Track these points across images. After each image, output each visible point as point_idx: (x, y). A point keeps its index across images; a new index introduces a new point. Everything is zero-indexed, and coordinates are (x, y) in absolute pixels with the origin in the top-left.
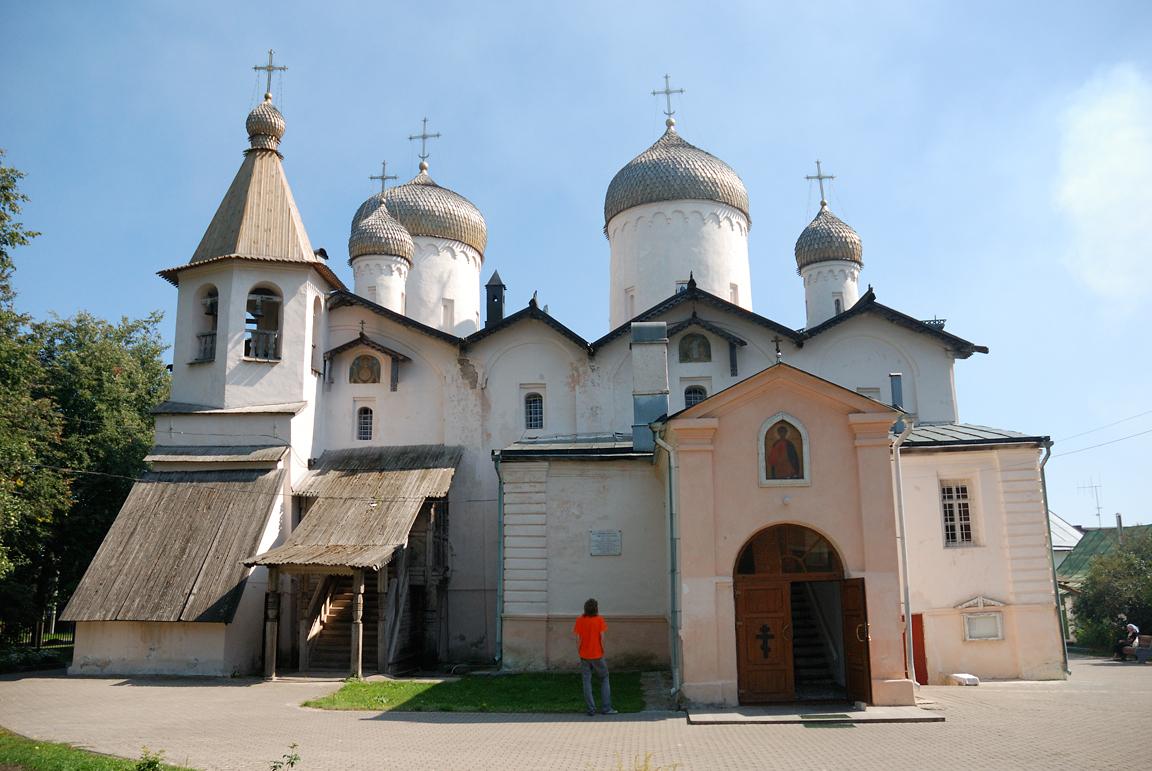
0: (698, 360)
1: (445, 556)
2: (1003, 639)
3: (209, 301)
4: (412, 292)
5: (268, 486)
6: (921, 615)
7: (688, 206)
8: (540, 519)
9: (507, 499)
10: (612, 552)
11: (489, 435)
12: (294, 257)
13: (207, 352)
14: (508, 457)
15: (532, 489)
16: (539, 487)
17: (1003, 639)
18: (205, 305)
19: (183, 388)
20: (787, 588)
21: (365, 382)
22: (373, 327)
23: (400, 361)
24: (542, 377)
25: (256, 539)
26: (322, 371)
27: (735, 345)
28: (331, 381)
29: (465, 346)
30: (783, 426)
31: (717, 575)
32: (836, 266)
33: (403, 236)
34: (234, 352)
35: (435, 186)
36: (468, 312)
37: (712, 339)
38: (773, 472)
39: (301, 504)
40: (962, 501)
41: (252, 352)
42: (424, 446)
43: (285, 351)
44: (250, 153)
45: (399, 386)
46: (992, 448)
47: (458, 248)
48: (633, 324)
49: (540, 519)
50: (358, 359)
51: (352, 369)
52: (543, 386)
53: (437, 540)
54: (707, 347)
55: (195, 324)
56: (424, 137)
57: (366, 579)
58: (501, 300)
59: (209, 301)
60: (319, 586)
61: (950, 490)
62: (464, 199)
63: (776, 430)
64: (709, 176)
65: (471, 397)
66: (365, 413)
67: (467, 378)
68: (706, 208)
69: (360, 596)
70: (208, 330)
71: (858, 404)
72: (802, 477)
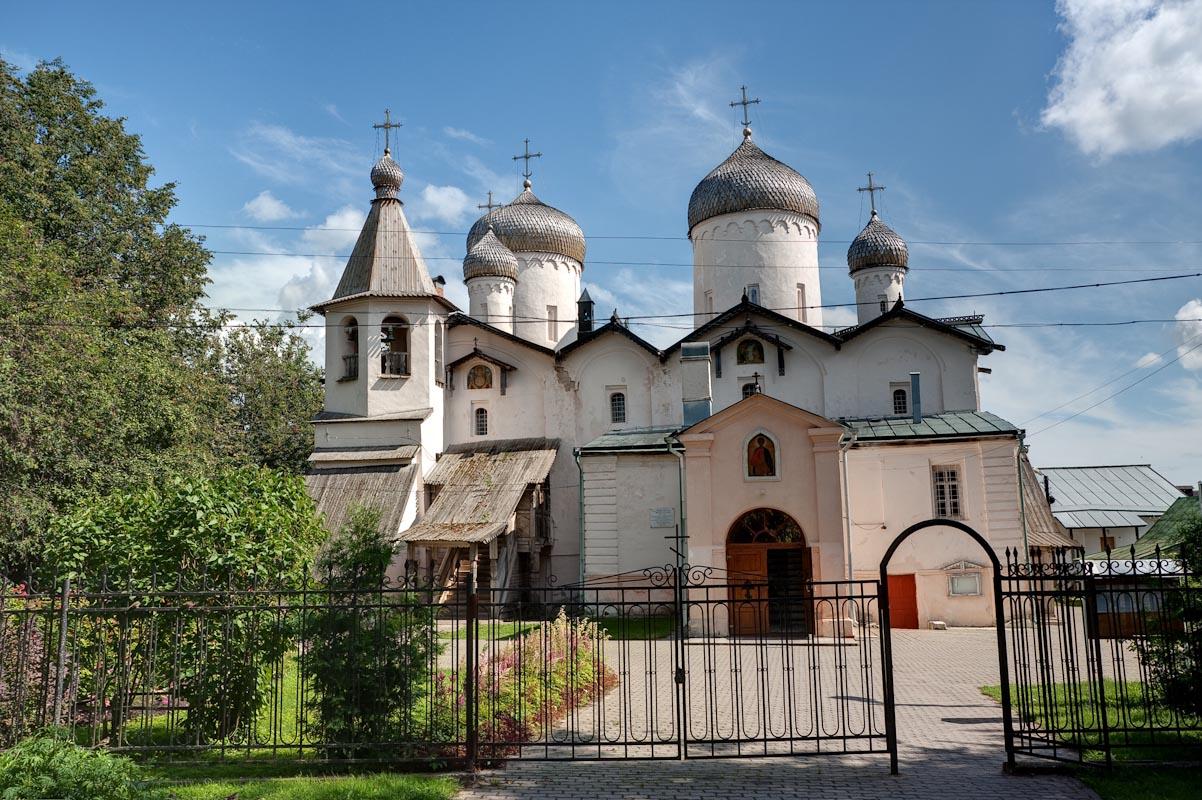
0: (753, 362)
1: (548, 528)
2: (981, 594)
3: (350, 329)
4: (517, 316)
5: (406, 475)
6: (913, 575)
7: (757, 216)
8: (612, 500)
9: (586, 485)
10: (667, 525)
11: (582, 429)
12: (415, 290)
13: (352, 373)
14: (588, 452)
15: (606, 477)
16: (610, 475)
17: (981, 594)
18: (348, 332)
19: (335, 399)
20: (765, 556)
21: (480, 388)
22: (484, 343)
23: (507, 370)
24: (623, 380)
25: (397, 521)
26: (444, 381)
27: (782, 349)
28: (452, 388)
29: (561, 356)
30: (761, 438)
31: (714, 544)
32: (881, 272)
33: (510, 258)
34: (373, 367)
35: (539, 204)
36: (567, 328)
37: (765, 344)
38: (753, 472)
39: (432, 490)
40: (951, 483)
41: (388, 370)
42: (530, 439)
43: (414, 368)
44: (376, 202)
45: (507, 390)
46: (975, 440)
47: (558, 260)
48: (683, 344)
49: (612, 500)
50: (474, 368)
51: (469, 378)
52: (625, 387)
53: (540, 516)
54: (760, 350)
55: (342, 348)
56: (527, 157)
57: (479, 548)
58: (590, 313)
59: (350, 329)
60: (446, 555)
61: (941, 474)
62: (563, 214)
63: (756, 440)
64: (777, 186)
65: (567, 397)
66: (481, 412)
67: (563, 383)
68: (774, 217)
69: (475, 563)
70: (351, 354)
71: (815, 422)
72: (774, 474)
